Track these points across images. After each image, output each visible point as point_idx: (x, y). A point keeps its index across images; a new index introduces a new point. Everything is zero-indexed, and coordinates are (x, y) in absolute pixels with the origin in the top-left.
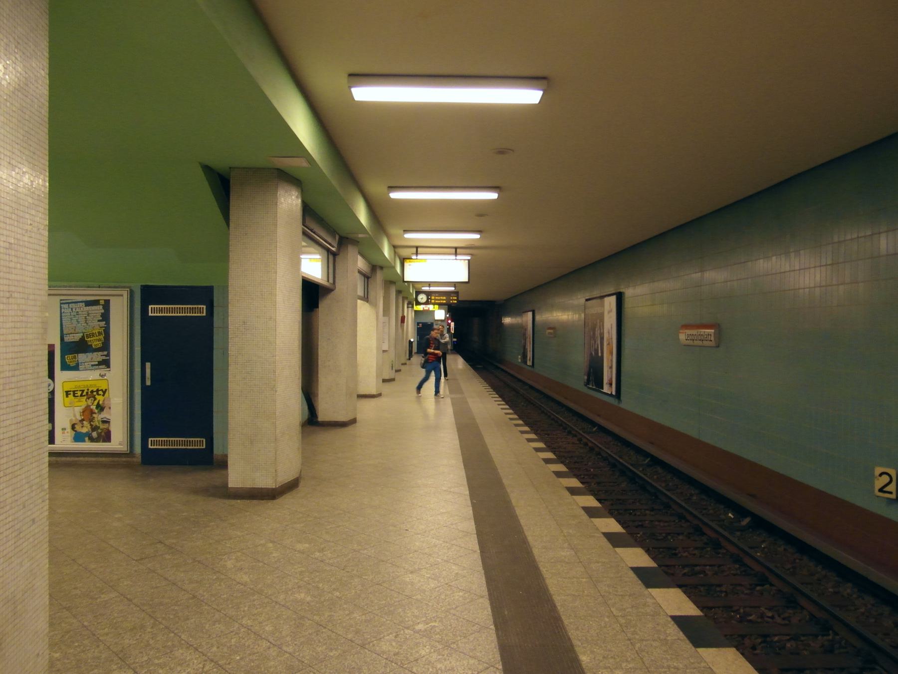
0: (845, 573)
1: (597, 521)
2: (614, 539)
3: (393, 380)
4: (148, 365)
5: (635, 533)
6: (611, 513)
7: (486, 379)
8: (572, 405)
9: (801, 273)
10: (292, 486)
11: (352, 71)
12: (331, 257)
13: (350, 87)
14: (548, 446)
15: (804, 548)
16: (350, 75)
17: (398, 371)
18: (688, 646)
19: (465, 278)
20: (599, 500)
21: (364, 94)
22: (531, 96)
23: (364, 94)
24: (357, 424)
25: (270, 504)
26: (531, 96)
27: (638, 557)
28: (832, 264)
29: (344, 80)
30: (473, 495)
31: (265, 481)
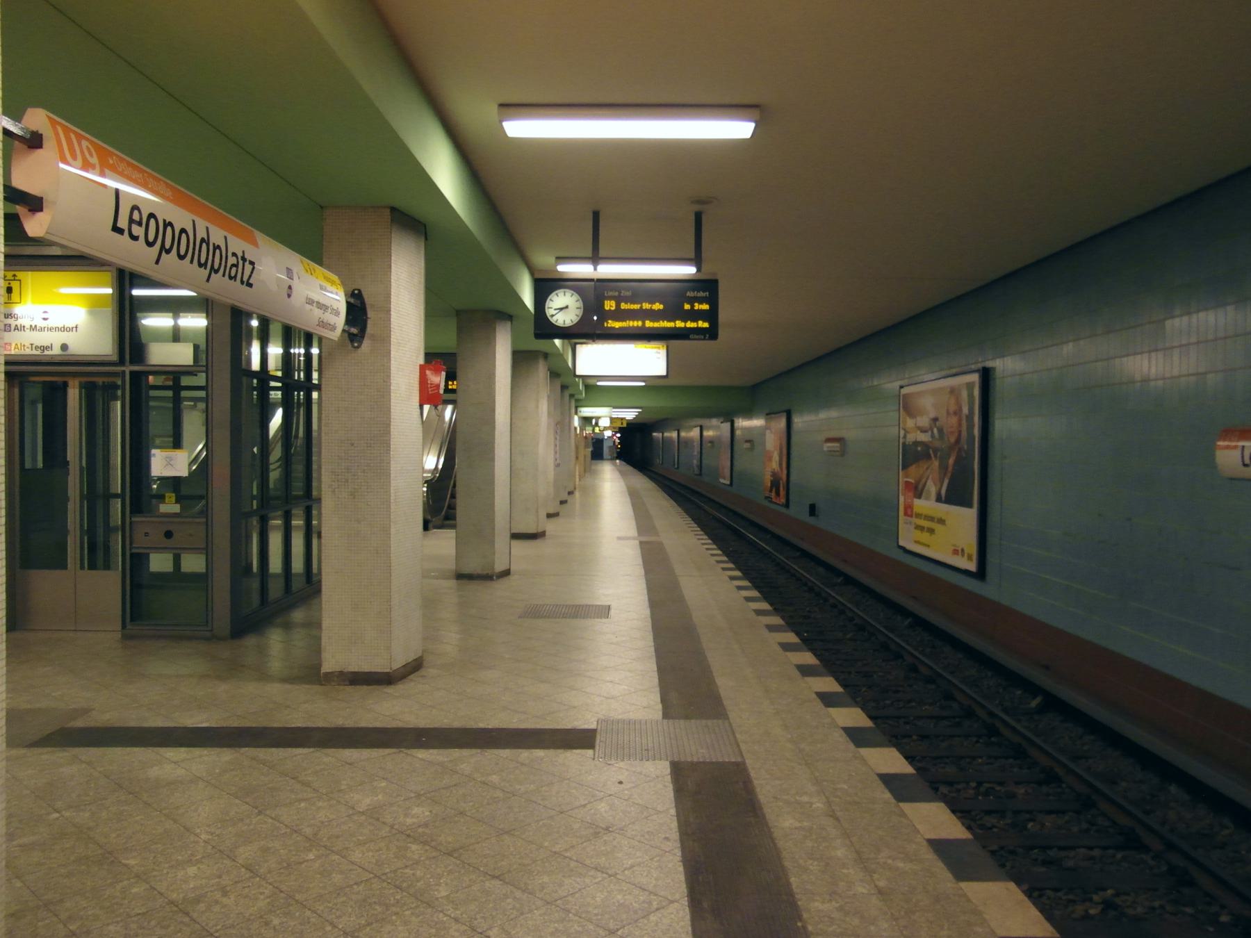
0: (1198, 790)
1: (834, 712)
2: (857, 737)
3: (556, 515)
4: (570, 364)
5: (888, 727)
6: (895, 739)
7: (645, 474)
8: (751, 517)
9: (1170, 352)
10: (415, 667)
11: (502, 101)
12: (920, 487)
13: (501, 121)
14: (804, 640)
15: (1115, 740)
16: (501, 105)
17: (562, 502)
18: (852, 746)
19: (663, 372)
20: (909, 758)
21: (519, 128)
22: (740, 129)
23: (519, 128)
24: (510, 577)
25: (390, 690)
26: (740, 129)
27: (891, 761)
28: (1198, 343)
29: (494, 109)
30: (661, 671)
31: (378, 665)
